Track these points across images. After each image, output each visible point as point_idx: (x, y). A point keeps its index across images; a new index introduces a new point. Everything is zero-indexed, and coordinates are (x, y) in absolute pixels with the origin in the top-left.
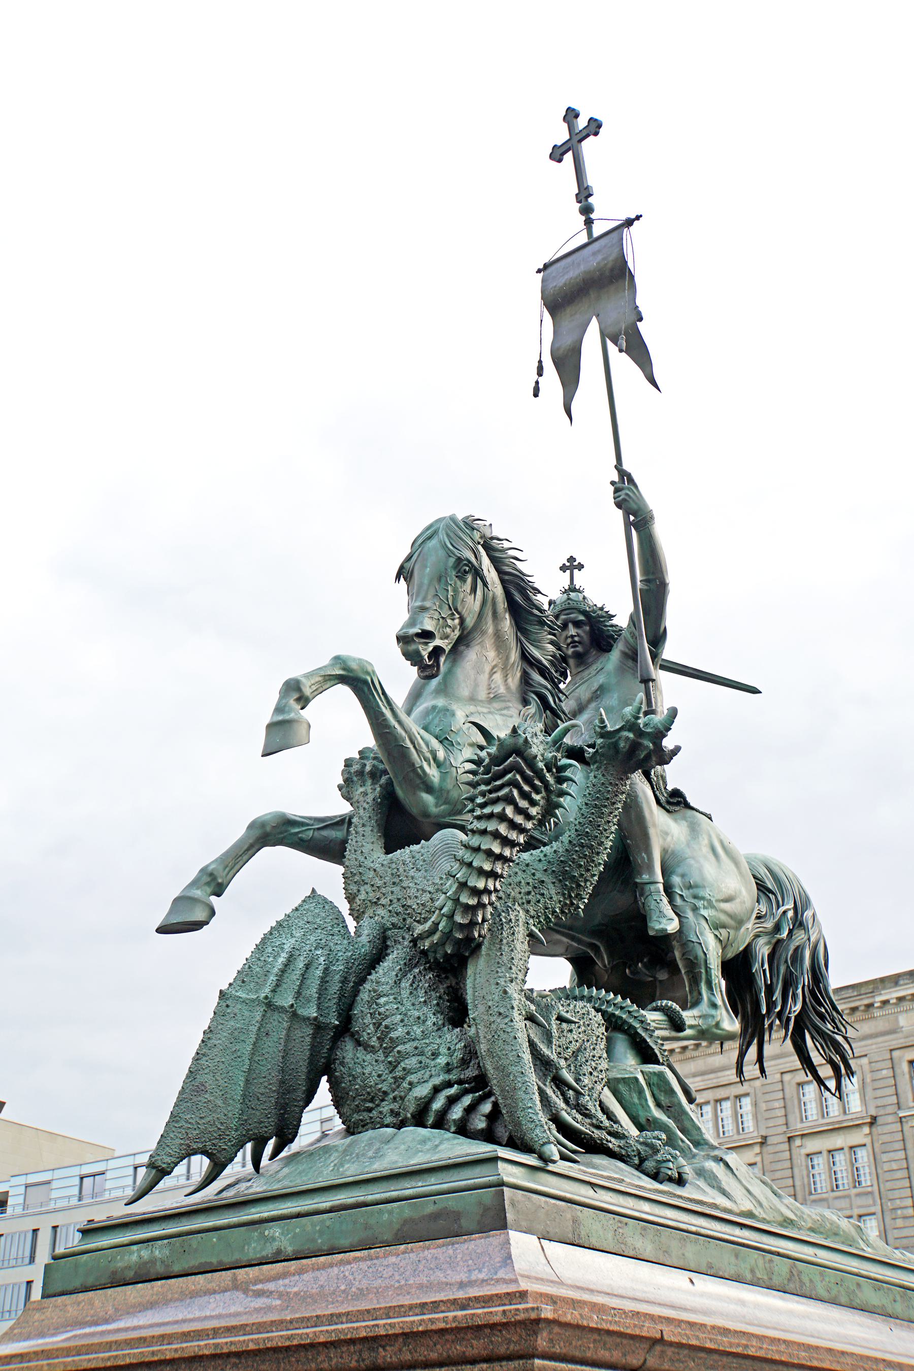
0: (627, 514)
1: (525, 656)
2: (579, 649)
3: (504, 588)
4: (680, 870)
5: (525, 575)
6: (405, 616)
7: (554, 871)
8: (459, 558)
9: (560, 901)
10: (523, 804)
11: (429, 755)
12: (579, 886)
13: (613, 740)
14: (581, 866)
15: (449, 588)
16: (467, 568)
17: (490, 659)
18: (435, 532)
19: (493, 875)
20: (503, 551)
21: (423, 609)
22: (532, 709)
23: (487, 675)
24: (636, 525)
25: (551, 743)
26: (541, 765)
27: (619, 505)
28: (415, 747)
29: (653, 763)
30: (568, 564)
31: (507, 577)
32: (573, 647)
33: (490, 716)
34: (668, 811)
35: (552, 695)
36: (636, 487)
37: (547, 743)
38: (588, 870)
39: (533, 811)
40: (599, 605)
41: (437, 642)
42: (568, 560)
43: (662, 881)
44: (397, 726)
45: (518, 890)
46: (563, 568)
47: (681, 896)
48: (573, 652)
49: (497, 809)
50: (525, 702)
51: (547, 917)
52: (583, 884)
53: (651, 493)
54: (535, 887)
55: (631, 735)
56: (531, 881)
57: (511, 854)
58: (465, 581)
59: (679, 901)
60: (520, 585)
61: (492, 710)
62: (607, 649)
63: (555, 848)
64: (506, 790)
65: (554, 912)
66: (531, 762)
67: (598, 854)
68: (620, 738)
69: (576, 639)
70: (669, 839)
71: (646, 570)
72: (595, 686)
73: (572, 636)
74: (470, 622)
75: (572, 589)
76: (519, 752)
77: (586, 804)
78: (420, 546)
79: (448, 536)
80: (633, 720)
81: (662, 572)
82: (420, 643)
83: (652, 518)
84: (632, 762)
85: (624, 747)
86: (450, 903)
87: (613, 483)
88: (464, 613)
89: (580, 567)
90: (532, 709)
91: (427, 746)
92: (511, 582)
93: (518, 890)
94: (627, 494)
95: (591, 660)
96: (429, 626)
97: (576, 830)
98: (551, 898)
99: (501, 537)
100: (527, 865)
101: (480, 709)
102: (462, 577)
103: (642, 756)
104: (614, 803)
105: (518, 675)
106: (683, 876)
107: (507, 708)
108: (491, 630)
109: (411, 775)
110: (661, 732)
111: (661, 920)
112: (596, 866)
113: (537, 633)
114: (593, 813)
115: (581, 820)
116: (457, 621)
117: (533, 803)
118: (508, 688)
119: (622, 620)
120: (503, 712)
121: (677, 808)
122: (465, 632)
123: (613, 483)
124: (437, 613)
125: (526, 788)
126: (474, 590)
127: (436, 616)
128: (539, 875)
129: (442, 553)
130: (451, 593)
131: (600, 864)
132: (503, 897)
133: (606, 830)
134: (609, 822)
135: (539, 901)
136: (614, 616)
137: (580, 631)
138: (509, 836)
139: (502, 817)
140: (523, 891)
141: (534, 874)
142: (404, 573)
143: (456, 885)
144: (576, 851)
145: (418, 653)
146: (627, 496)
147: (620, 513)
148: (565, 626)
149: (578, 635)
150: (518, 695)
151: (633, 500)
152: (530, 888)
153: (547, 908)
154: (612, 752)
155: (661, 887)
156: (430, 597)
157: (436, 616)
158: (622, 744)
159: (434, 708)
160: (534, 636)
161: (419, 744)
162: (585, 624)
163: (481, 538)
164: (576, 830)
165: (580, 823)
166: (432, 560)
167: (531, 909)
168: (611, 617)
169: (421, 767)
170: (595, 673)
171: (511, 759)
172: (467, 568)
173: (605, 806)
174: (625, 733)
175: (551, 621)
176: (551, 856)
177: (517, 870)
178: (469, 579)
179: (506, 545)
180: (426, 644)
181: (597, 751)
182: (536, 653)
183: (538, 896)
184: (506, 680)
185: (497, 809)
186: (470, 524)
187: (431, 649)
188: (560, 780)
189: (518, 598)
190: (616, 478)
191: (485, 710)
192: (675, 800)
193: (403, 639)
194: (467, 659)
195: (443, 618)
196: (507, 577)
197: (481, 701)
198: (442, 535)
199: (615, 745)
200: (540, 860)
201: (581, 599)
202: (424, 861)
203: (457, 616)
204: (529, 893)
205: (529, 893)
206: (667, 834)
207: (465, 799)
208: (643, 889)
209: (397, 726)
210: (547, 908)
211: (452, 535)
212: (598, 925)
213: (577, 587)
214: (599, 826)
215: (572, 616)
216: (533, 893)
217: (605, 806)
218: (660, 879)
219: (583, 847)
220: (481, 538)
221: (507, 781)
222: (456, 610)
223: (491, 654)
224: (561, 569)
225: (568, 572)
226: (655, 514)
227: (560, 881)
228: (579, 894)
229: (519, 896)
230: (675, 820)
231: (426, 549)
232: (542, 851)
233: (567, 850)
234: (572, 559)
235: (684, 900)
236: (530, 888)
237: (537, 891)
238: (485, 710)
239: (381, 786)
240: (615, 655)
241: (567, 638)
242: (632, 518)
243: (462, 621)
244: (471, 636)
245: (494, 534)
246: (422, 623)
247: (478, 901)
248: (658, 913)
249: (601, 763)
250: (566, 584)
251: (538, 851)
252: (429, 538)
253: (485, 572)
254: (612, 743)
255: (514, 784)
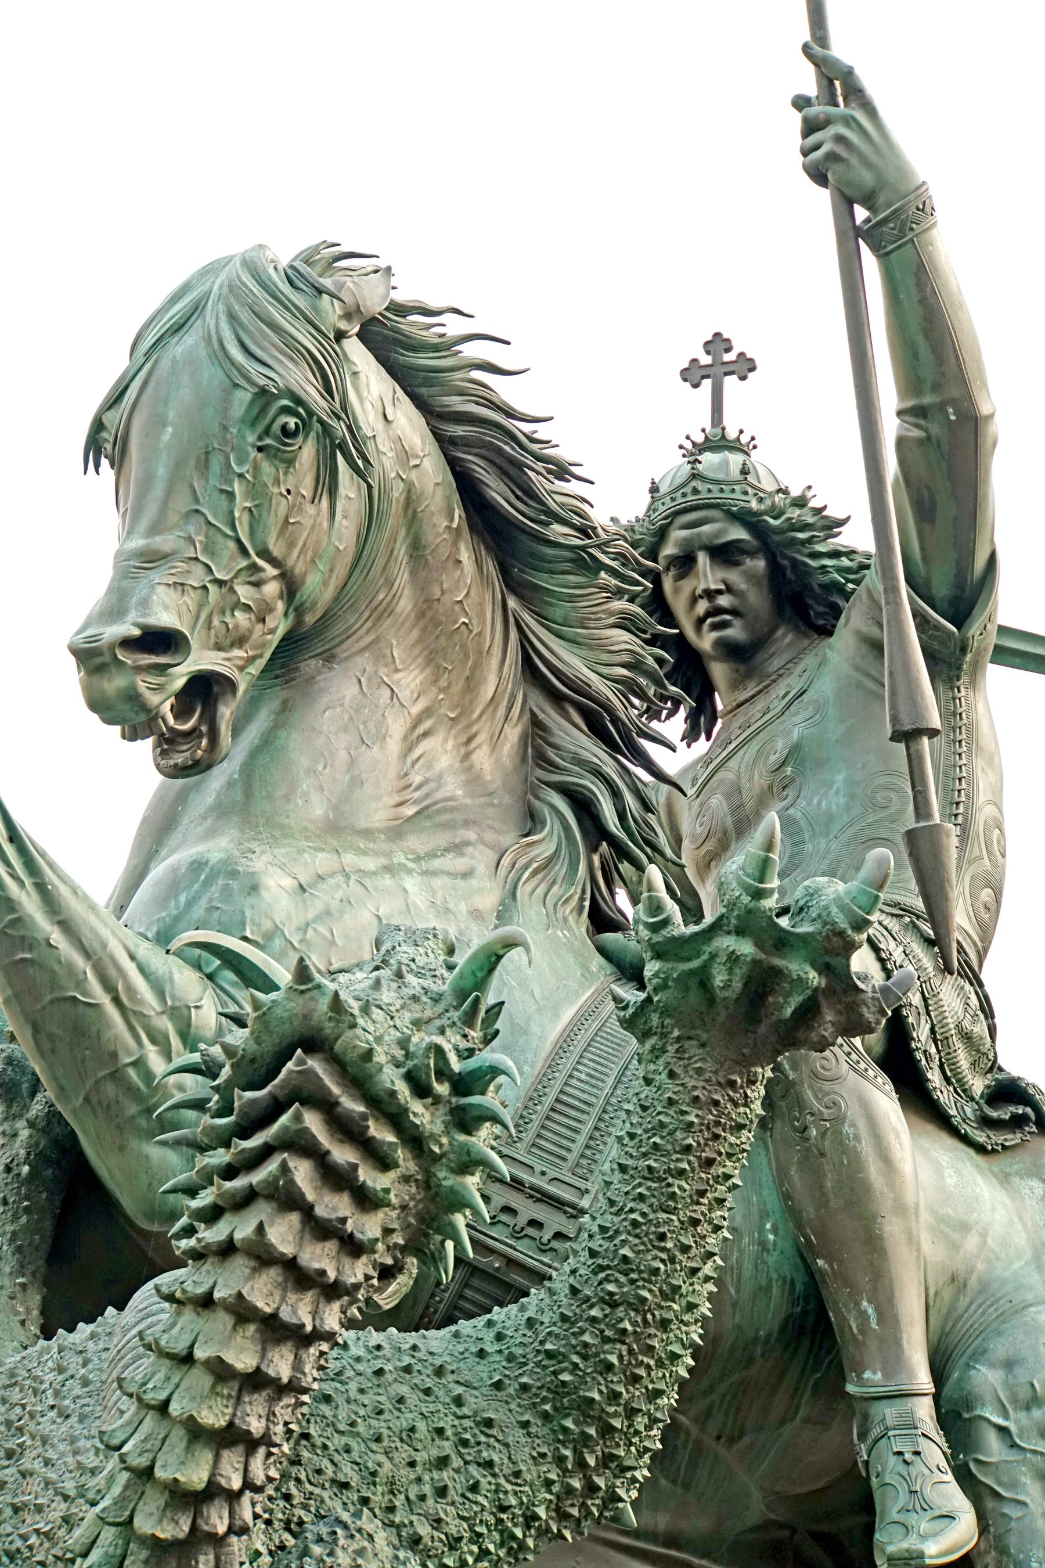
0: (845, 202)
1: (531, 669)
2: (736, 632)
3: (453, 463)
4: (1000, 1349)
5: (510, 413)
6: (96, 581)
7: (525, 1388)
8: (263, 391)
9: (548, 1484)
10: (334, 1206)
11: (167, 1025)
12: (607, 1430)
13: (695, 964)
14: (609, 1367)
15: (237, 487)
16: (292, 422)
17: (404, 695)
18: (197, 309)
19: (231, 1437)
20: (445, 346)
21: (152, 559)
22: (547, 842)
23: (394, 745)
24: (872, 234)
25: (449, 999)
26: (392, 1079)
27: (818, 175)
28: (117, 1001)
29: (827, 1031)
30: (706, 360)
31: (459, 430)
32: (715, 627)
33: (387, 881)
34: (980, 1149)
35: (616, 794)
36: (871, 111)
37: (437, 999)
38: (636, 1379)
39: (368, 1227)
40: (795, 492)
41: (201, 659)
42: (708, 347)
43: (929, 1387)
44: (57, 937)
45: (404, 1453)
46: (692, 374)
47: (1003, 1430)
48: (718, 643)
49: (241, 1228)
50: (531, 820)
51: (508, 1537)
52: (617, 1423)
53: (920, 133)
54: (465, 1443)
55: (746, 948)
56: (447, 1423)
57: (298, 1365)
58: (290, 462)
59: (994, 1449)
60: (500, 451)
61: (400, 858)
62: (822, 627)
63: (531, 1313)
64: (271, 1166)
65: (530, 1519)
66: (357, 1076)
67: (664, 1325)
68: (713, 956)
69: (724, 601)
70: (971, 1243)
71: (911, 380)
72: (781, 747)
73: (710, 594)
74: (319, 587)
75: (718, 442)
76: (312, 1043)
77: (623, 1168)
78: (148, 355)
79: (232, 317)
80: (746, 899)
81: (963, 382)
82: (139, 669)
83: (925, 209)
84: (762, 1029)
85: (727, 985)
86: (109, 1534)
87: (800, 103)
88: (296, 563)
89: (745, 366)
90: (547, 842)
91: (160, 994)
92: (466, 443)
93: (404, 1453)
94: (840, 139)
95: (775, 664)
96: (166, 613)
97: (593, 1254)
98: (517, 1474)
99: (434, 304)
100: (439, 1371)
101: (349, 859)
102: (278, 445)
103: (789, 1011)
104: (710, 1163)
105: (513, 734)
106: (1009, 1365)
107: (457, 848)
108: (405, 604)
109: (110, 1090)
110: (841, 934)
111: (912, 1519)
112: (660, 1364)
113: (572, 598)
114: (641, 1198)
115: (607, 1220)
116: (272, 589)
117: (366, 1200)
118: (473, 780)
119: (858, 536)
120: (437, 863)
121: (1012, 1139)
122: (310, 619)
123: (800, 103)
124: (199, 570)
125: (342, 1155)
126: (327, 483)
127: (197, 577)
128: (473, 1402)
129: (212, 375)
130: (241, 502)
131: (674, 1357)
132: (355, 1480)
133: (685, 1249)
134: (695, 1223)
135: (475, 1488)
136: (842, 523)
137: (734, 576)
138: (285, 1315)
139: (262, 1256)
140: (420, 1457)
141: (458, 1401)
142: (103, 444)
143: (125, 1475)
144: (594, 1320)
145: (133, 698)
146: (842, 141)
147: (822, 198)
148: (685, 563)
149: (729, 589)
150: (507, 800)
151: (861, 156)
152: (447, 1447)
153: (503, 1509)
154: (695, 998)
155: (924, 1410)
156: (173, 518)
157: (197, 577)
158: (719, 978)
159: (197, 865)
160: (559, 610)
161: (131, 990)
162: (752, 554)
163: (348, 316)
164: (593, 1254)
165: (603, 1229)
166: (183, 396)
167: (448, 1514)
168: (832, 526)
169: (139, 1063)
170: (778, 706)
171: (290, 1065)
172: (292, 422)
173: (681, 1173)
174: (726, 943)
175: (620, 556)
176: (518, 1337)
177: (404, 1390)
178: (307, 451)
179: (453, 326)
180: (162, 669)
181: (649, 1000)
182: (574, 663)
183: (473, 1469)
184: (467, 755)
185: (241, 1228)
186: (315, 273)
187: (180, 683)
188: (465, 1121)
189: (497, 491)
190: (810, 88)
191: (370, 864)
192: (1004, 1113)
193: (91, 658)
194: (325, 700)
195: (220, 583)
196: (459, 430)
197: (367, 833)
198: (214, 318)
199: (702, 978)
200: (482, 1354)
201: (735, 472)
202: (85, 1383)
203: (271, 571)
204: (443, 1462)
205: (443, 1462)
206: (964, 1227)
207: (173, 1191)
208: (866, 1416)
209: (57, 937)
210: (503, 1509)
211: (245, 316)
212: (753, 1530)
213: (732, 434)
214: (662, 1237)
215: (706, 528)
216: (456, 1462)
217: (681, 1173)
218: (924, 1380)
219: (614, 1305)
220: (348, 316)
221: (277, 1137)
222: (265, 554)
223: (410, 680)
224: (685, 375)
225: (707, 384)
226: (939, 196)
227: (546, 1417)
228: (613, 1457)
229: (406, 1474)
230: (1004, 1179)
231: (165, 364)
232: (490, 1324)
233: (564, 1318)
234: (718, 343)
235: (1014, 1445)
236: (447, 1447)
237: (470, 1453)
238: (370, 864)
239: (31, 1124)
240: (841, 647)
241: (694, 600)
242: (861, 214)
243: (291, 586)
244: (337, 629)
245: (399, 296)
246: (145, 604)
247: (194, 1528)
248: (903, 1498)
249: (663, 1036)
250: (697, 421)
251: (481, 1321)
252: (178, 328)
253: (368, 420)
254: (692, 972)
255: (300, 1144)
